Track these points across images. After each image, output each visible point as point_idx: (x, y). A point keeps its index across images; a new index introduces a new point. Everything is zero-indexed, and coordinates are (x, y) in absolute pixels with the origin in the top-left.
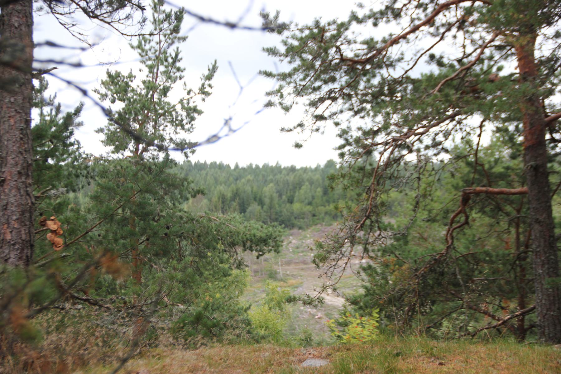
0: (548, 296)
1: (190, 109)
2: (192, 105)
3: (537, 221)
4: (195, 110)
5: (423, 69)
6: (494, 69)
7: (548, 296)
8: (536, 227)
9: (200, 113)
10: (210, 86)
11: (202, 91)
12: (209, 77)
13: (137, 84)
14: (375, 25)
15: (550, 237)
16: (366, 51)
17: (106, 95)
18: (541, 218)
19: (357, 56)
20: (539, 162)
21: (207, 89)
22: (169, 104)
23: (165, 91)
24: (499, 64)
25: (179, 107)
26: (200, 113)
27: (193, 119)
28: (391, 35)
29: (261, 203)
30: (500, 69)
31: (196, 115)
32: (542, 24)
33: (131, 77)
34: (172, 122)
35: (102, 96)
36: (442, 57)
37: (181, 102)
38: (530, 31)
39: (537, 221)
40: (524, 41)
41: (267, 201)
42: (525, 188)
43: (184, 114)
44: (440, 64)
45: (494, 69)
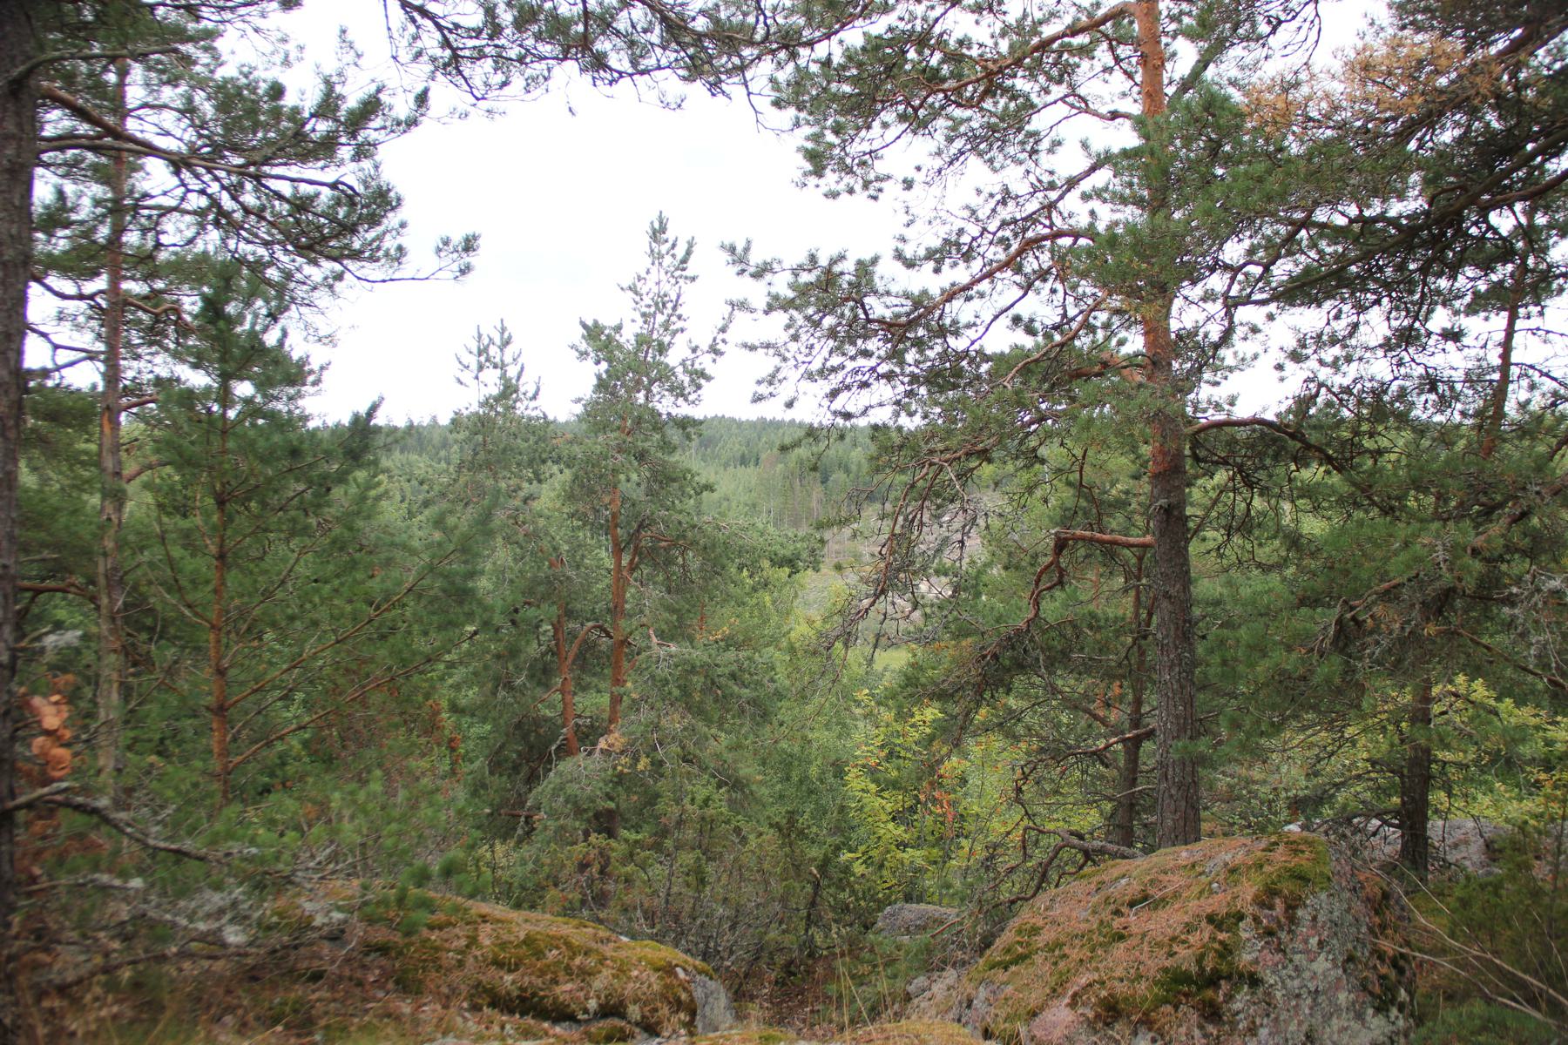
0: (1177, 717)
1: (696, 372)
2: (697, 366)
3: (1167, 596)
4: (702, 374)
5: (1002, 340)
6: (1114, 342)
7: (1177, 717)
8: (1165, 604)
9: (708, 378)
10: (724, 341)
11: (714, 350)
12: (723, 330)
13: (627, 338)
14: (937, 271)
15: (1185, 621)
16: (907, 309)
17: (586, 353)
18: (1172, 592)
19: (898, 316)
20: (1174, 501)
21: (721, 346)
22: (667, 366)
23: (662, 349)
24: (1120, 335)
25: (679, 370)
26: (708, 378)
27: (699, 387)
28: (953, 285)
29: (847, 471)
30: (1121, 343)
31: (702, 381)
32: (1182, 280)
33: (618, 328)
34: (671, 390)
35: (582, 354)
36: (1032, 320)
37: (683, 363)
38: (1164, 292)
39: (1167, 596)
40: (1149, 311)
41: (854, 468)
42: (1148, 539)
43: (687, 380)
44: (1030, 331)
45: (1114, 342)
